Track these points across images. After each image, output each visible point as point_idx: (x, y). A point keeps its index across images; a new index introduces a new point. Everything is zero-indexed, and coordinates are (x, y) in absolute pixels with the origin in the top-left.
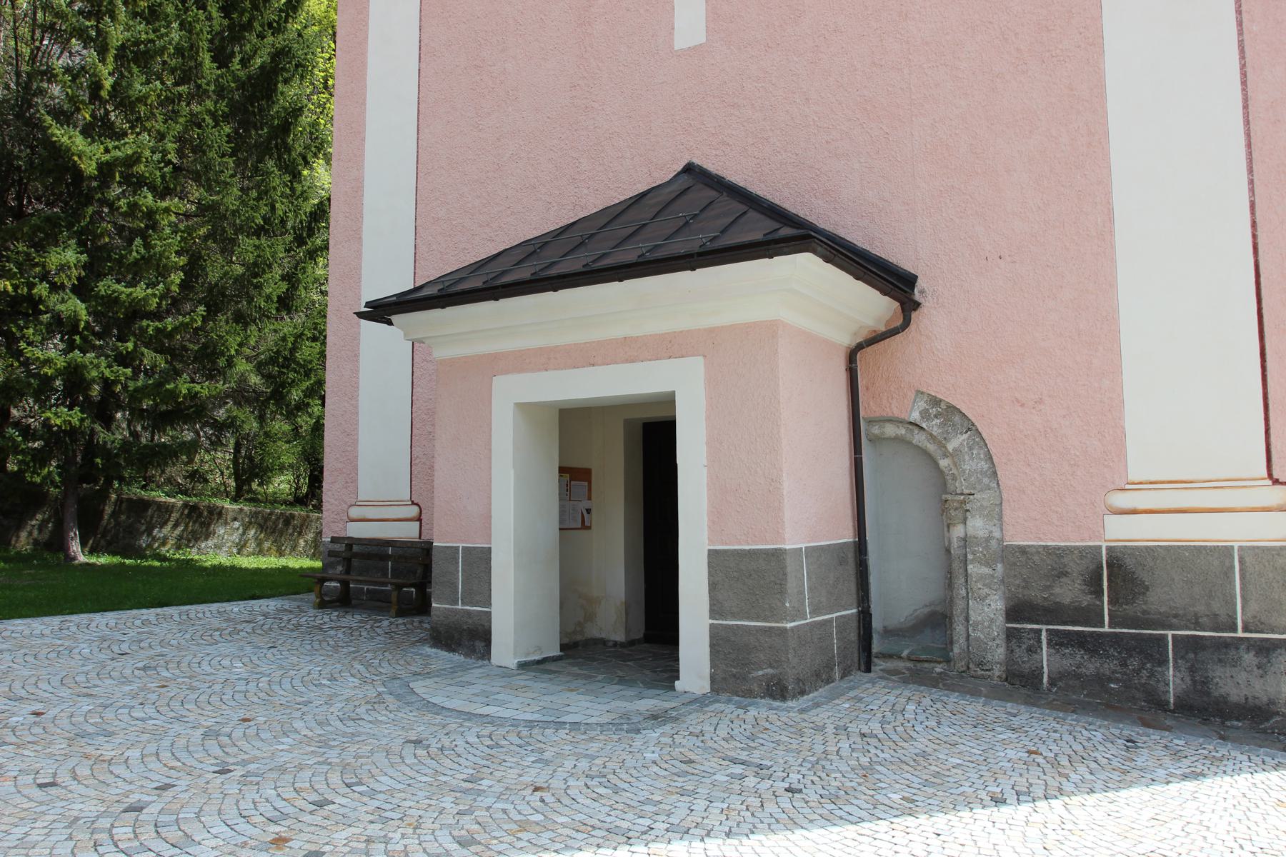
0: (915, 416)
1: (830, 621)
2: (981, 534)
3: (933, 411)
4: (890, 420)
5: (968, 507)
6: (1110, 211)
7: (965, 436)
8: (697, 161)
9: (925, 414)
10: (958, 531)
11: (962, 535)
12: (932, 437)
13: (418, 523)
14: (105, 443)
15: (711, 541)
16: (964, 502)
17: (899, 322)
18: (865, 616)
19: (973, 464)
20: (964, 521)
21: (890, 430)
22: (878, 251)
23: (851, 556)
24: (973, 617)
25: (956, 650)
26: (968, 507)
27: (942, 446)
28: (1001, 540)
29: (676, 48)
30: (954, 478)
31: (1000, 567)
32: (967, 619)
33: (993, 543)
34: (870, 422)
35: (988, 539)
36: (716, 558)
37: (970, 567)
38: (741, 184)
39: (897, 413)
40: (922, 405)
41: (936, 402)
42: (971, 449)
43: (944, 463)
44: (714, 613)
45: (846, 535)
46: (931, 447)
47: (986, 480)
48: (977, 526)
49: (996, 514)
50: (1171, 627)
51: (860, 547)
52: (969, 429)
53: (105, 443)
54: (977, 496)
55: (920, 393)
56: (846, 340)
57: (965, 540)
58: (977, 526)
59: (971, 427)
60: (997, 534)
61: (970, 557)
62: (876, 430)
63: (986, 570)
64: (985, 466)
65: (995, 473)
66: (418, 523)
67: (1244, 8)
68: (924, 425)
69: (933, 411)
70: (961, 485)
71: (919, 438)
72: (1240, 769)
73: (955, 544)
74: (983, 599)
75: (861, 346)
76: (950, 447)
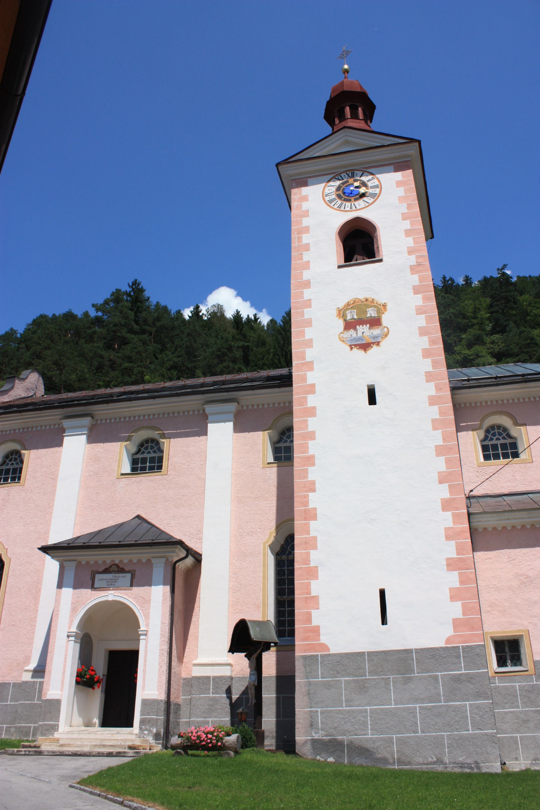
23: (163, 707)
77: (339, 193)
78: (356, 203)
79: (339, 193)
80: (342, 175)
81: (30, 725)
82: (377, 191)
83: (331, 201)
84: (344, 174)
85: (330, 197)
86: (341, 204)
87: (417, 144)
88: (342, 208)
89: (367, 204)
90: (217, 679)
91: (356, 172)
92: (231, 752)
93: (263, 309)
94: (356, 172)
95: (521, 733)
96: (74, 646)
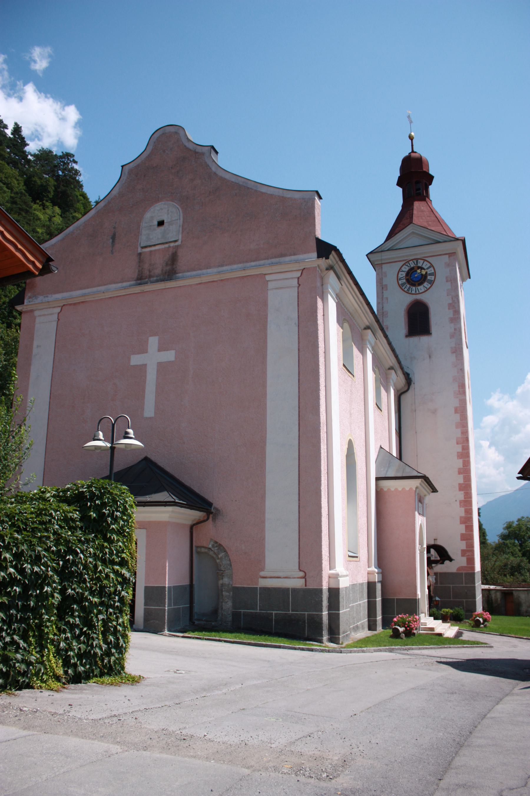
0: (210, 546)
1: (180, 608)
2: (227, 583)
3: (215, 545)
4: (203, 547)
5: (223, 575)
6: (265, 491)
7: (224, 553)
8: (149, 456)
9: (213, 546)
10: (221, 582)
11: (222, 583)
12: (215, 553)
13: (304, 580)
14: (124, 574)
15: (146, 583)
16: (222, 573)
17: (206, 518)
18: (191, 608)
19: (225, 562)
20: (222, 579)
21: (203, 550)
22: (202, 494)
23: (188, 589)
24: (224, 608)
25: (219, 618)
26: (223, 575)
27: (217, 556)
28: (232, 585)
29: (134, 637)
30: (221, 566)
31: (231, 593)
32: (222, 608)
33: (230, 586)
34: (197, 547)
35: (229, 584)
36: (146, 588)
37: (223, 593)
38: (162, 467)
39: (205, 545)
40: (212, 543)
41: (216, 542)
42: (225, 557)
43: (218, 561)
44: (145, 606)
45: (187, 582)
46: (215, 556)
47: (229, 567)
48: (226, 580)
49: (231, 577)
50: (274, 610)
51: (191, 585)
52: (225, 551)
53: (124, 574)
54: (226, 571)
55: (211, 539)
56: (190, 523)
57: (222, 585)
58: (226, 580)
59: (225, 551)
60: (231, 583)
61: (223, 590)
62: (199, 550)
63: (227, 594)
64: (228, 562)
65: (231, 565)
66: (304, 580)
67: (300, 439)
68: (213, 549)
69: (215, 545)
70: (222, 568)
71: (211, 553)
72: (390, 702)
73: (220, 586)
74: (227, 602)
75: (194, 525)
76: (220, 556)
77: (407, 278)
78: (419, 288)
79: (407, 278)
80: (410, 262)
81: (479, 598)
82: (432, 278)
83: (403, 284)
84: (412, 262)
85: (402, 281)
86: (409, 288)
87: (461, 243)
88: (410, 292)
89: (426, 289)
90: (222, 548)
91: (419, 261)
92: (112, 661)
93: (331, 251)
94: (419, 261)
95: (307, 612)
96: (339, 584)
